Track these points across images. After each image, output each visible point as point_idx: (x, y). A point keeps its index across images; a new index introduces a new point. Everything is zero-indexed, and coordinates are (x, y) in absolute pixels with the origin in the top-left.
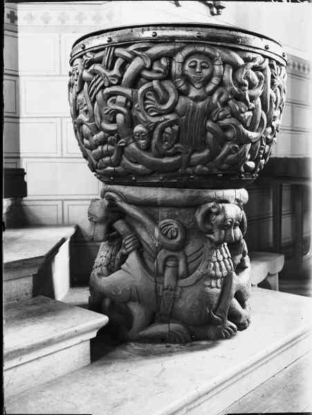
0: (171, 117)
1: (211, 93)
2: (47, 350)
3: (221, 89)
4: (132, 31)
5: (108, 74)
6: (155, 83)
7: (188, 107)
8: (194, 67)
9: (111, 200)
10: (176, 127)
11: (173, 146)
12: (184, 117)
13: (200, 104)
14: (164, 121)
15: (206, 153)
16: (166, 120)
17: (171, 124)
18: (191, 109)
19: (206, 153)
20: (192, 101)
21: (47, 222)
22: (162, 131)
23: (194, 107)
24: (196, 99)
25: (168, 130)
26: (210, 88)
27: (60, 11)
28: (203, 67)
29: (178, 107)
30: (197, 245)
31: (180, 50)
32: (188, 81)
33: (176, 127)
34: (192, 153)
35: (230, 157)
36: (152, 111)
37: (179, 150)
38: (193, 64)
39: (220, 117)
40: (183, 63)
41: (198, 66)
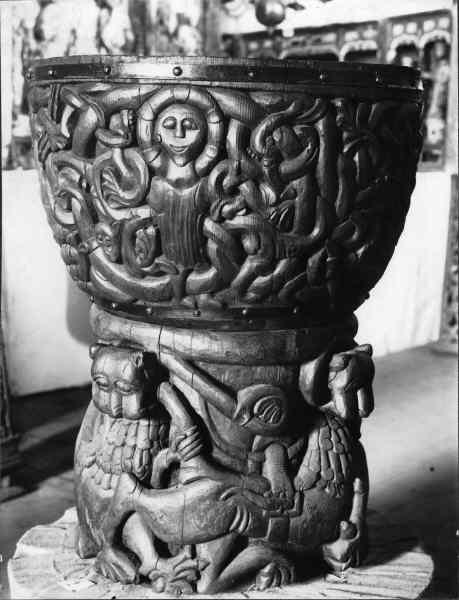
0: (144, 212)
2: (30, 10)
3: (222, 166)
6: (117, 151)
7: (166, 198)
8: (173, 127)
9: (109, 503)
10: (151, 230)
12: (162, 215)
13: (186, 192)
15: (210, 274)
17: (145, 223)
19: (210, 274)
20: (171, 188)
23: (177, 198)
24: (178, 184)
26: (202, 163)
27: (105, 204)
28: (184, 129)
30: (227, 405)
32: (164, 152)
33: (151, 230)
34: (188, 272)
37: (162, 269)
41: (179, 127)
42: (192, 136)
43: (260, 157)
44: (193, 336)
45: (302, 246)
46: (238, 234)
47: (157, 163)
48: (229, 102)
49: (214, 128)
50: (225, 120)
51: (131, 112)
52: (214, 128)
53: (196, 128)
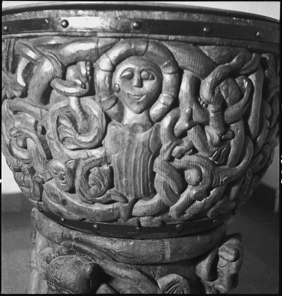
6: (73, 101)
8: (130, 77)
24: (133, 129)
26: (156, 109)
33: (106, 167)
36: (70, 143)
38: (127, 73)
39: (173, 155)
42: (148, 85)
46: (181, 171)
50: (179, 73)
51: (88, 63)
53: (153, 78)
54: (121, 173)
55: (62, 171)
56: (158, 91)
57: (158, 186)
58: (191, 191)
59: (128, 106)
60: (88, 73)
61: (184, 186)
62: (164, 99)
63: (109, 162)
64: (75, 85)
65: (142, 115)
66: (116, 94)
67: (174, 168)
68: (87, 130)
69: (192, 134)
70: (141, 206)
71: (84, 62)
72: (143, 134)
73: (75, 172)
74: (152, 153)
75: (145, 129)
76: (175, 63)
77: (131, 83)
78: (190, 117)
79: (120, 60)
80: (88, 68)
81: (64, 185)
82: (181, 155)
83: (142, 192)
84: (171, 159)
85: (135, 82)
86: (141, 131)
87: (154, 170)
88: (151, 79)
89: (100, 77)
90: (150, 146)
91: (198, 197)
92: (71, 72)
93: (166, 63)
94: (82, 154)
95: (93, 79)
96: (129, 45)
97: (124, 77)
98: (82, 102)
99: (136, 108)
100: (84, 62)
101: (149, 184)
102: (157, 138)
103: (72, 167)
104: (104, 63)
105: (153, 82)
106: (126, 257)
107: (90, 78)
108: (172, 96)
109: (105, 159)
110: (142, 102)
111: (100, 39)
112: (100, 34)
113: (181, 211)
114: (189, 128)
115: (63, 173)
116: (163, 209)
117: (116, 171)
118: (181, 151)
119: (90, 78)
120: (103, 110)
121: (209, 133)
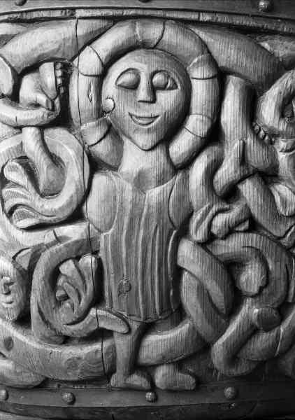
1: (187, 164)
4: (125, 380)
5: (104, 234)
6: (30, 135)
8: (134, 86)
10: (88, 260)
11: (87, 312)
14: (53, 244)
16: (58, 240)
18: (129, 207)
21: (137, 80)
22: (54, 275)
24: (140, 182)
25: (68, 268)
26: (181, 145)
28: (153, 90)
29: (93, 207)
31: (92, 39)
33: (88, 260)
35: (262, 341)
36: (24, 216)
37: (102, 324)
38: (128, 78)
39: (214, 231)
40: (101, 77)
42: (167, 100)
43: (274, 135)
44: (201, 138)
45: (223, 343)
46: (231, 267)
47: (102, 150)
48: (227, 50)
49: (201, 91)
50: (220, 77)
51: (59, 66)
52: (201, 91)
53: (174, 87)
54: (118, 268)
55: (8, 276)
56: (184, 110)
57: (190, 299)
58: (250, 310)
59: (130, 138)
60: (59, 81)
61: (236, 298)
62: (196, 125)
63: (94, 248)
64: (37, 105)
65: (153, 154)
66: (108, 117)
67: (216, 258)
68: (52, 192)
69: (249, 190)
70: (158, 342)
71: (52, 64)
72: (158, 190)
73: (30, 279)
74: (174, 227)
75: (161, 181)
76: (212, 61)
77: (135, 95)
78: (243, 160)
79: (115, 56)
80: (59, 73)
81: (9, 306)
82: (230, 231)
83: (157, 307)
84: (210, 238)
85: (143, 93)
86: (154, 184)
87: (180, 262)
88: (171, 89)
89: (80, 90)
90: (171, 213)
91: (267, 324)
92: (28, 88)
93: (196, 60)
94: (45, 237)
95: (67, 93)
96: (131, 31)
97: (121, 86)
98: (46, 137)
99: (145, 139)
100: (52, 64)
101: (171, 293)
102: (183, 196)
103: (25, 265)
104: (89, 61)
105: (174, 93)
106: (228, 43)
107: (62, 91)
108: (208, 118)
109: (89, 245)
110: (156, 128)
111: (79, 21)
112: (79, 13)
113: (234, 356)
114: (242, 180)
115: (8, 279)
116: (201, 347)
117: (109, 267)
118: (226, 224)
119: (62, 91)
120: (84, 148)
121: (279, 193)
